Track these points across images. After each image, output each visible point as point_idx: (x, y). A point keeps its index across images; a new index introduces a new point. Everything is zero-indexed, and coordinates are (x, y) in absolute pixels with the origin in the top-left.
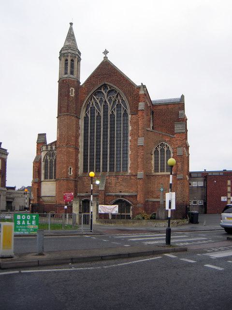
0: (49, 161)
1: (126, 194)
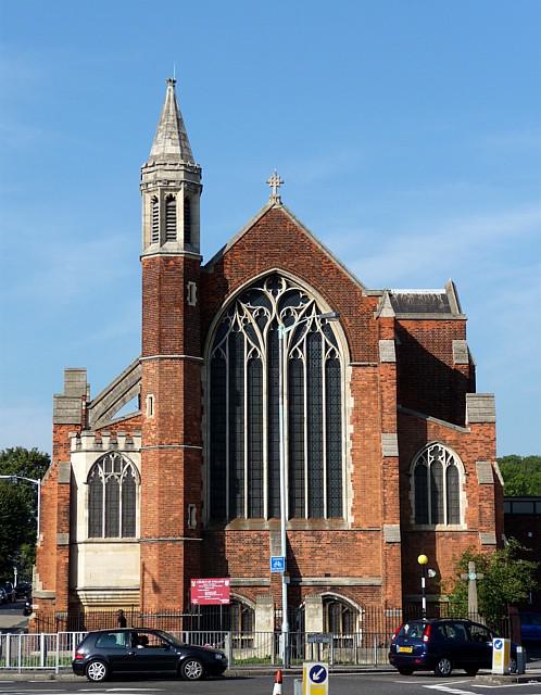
0: (104, 481)
1: (346, 581)
